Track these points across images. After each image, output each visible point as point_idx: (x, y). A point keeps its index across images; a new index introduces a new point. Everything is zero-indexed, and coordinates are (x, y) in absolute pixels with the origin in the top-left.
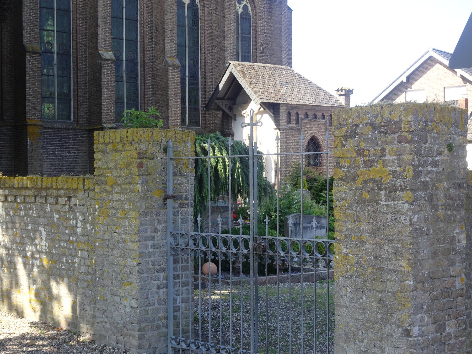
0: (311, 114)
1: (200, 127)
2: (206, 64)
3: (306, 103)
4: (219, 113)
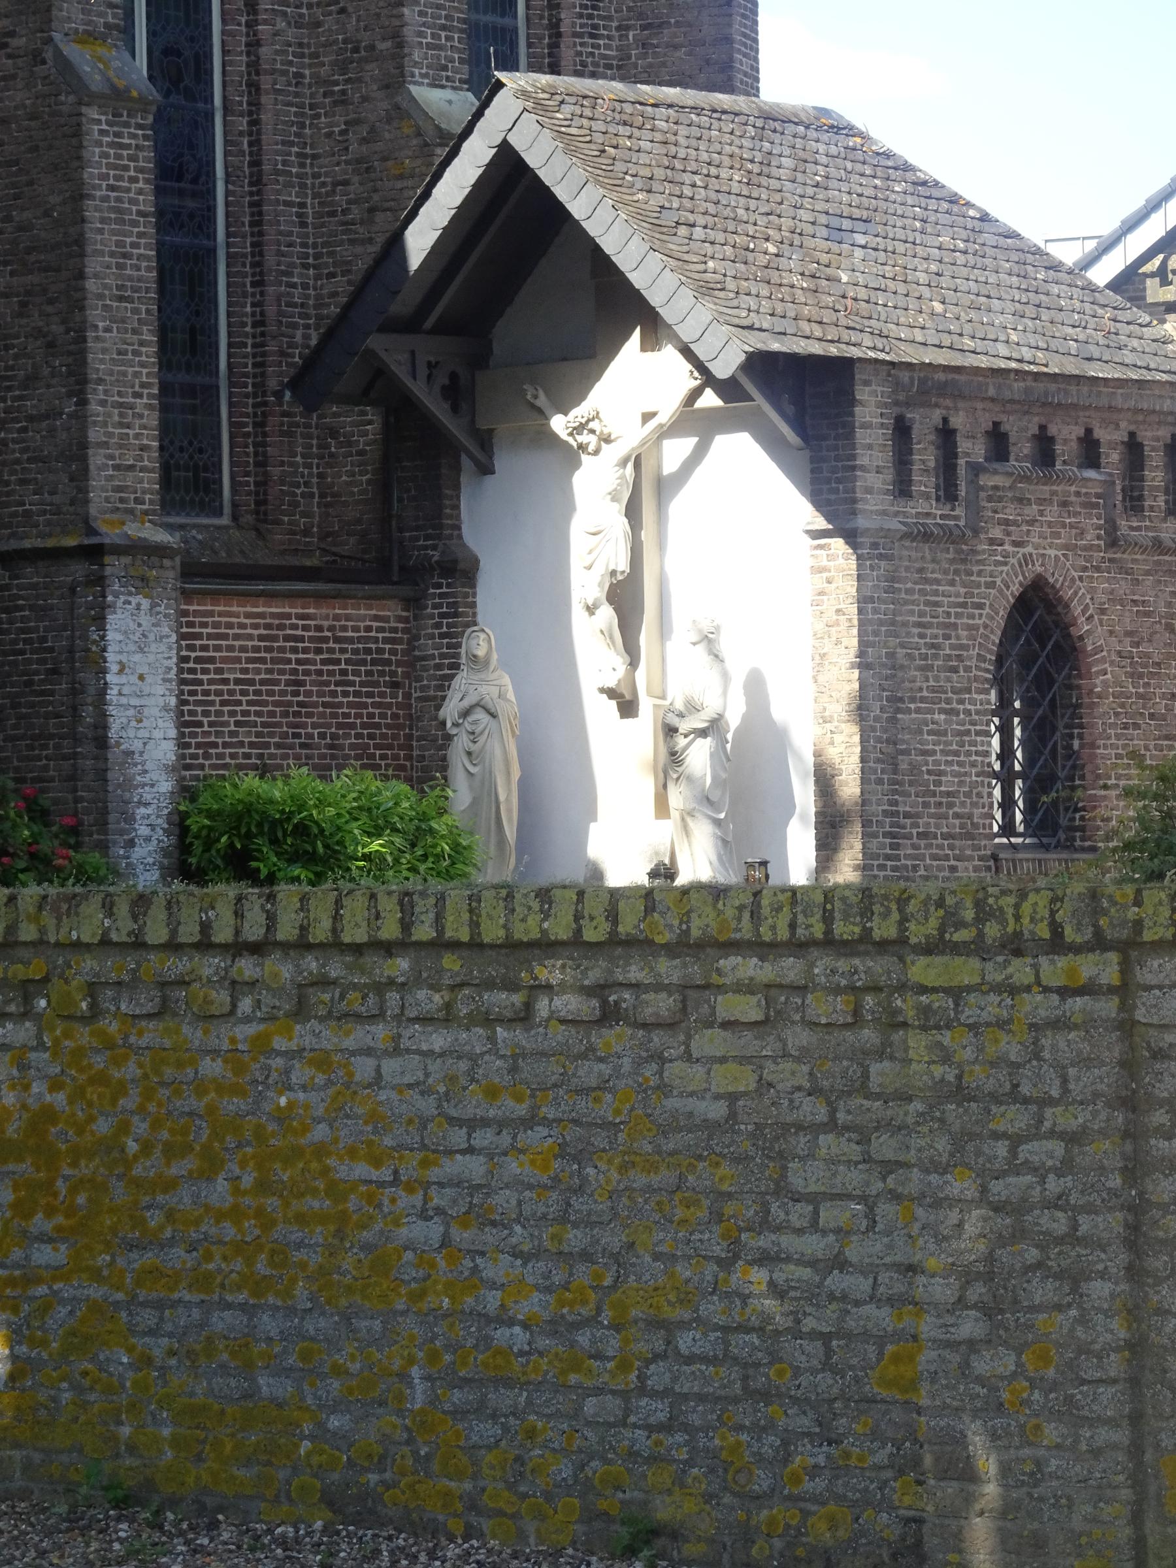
0: (1021, 431)
1: (225, 521)
2: (266, 82)
3: (998, 356)
4: (365, 426)
